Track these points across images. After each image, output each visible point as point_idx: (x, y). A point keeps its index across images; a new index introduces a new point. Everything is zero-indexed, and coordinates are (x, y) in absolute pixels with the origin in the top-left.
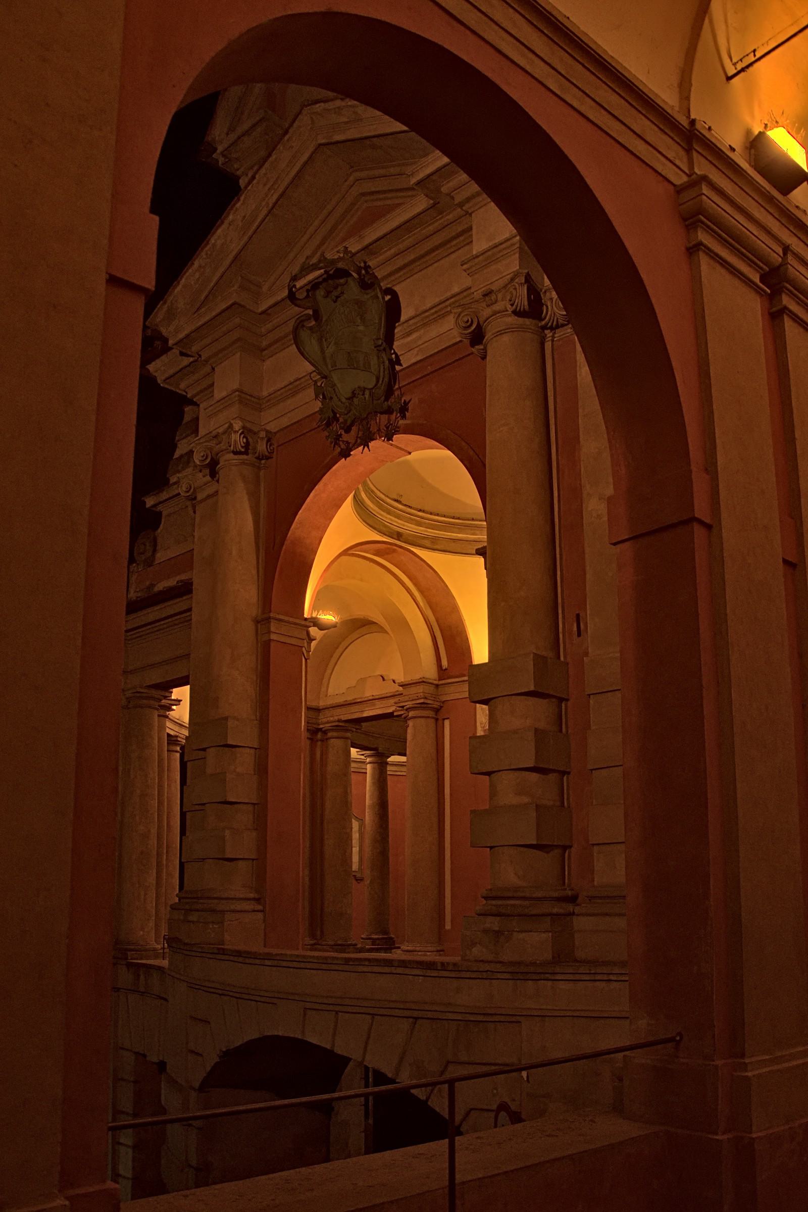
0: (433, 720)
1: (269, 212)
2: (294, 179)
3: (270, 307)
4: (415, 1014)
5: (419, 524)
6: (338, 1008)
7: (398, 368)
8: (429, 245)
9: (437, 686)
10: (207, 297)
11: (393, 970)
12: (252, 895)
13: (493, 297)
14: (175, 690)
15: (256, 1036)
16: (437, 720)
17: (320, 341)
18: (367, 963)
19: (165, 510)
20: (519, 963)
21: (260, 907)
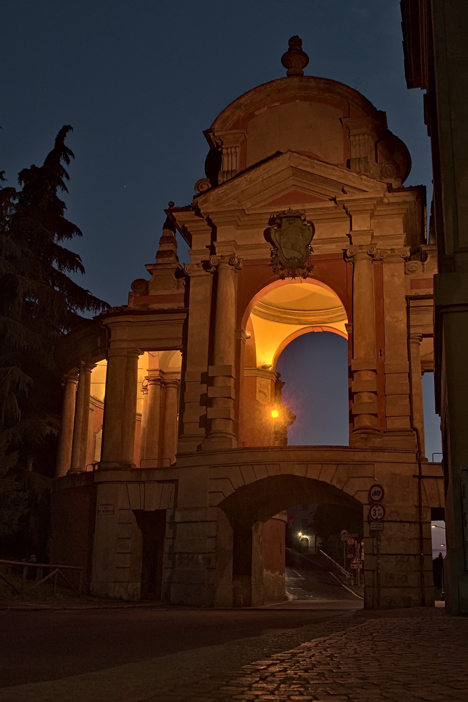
8: (326, 217)
17: (280, 235)
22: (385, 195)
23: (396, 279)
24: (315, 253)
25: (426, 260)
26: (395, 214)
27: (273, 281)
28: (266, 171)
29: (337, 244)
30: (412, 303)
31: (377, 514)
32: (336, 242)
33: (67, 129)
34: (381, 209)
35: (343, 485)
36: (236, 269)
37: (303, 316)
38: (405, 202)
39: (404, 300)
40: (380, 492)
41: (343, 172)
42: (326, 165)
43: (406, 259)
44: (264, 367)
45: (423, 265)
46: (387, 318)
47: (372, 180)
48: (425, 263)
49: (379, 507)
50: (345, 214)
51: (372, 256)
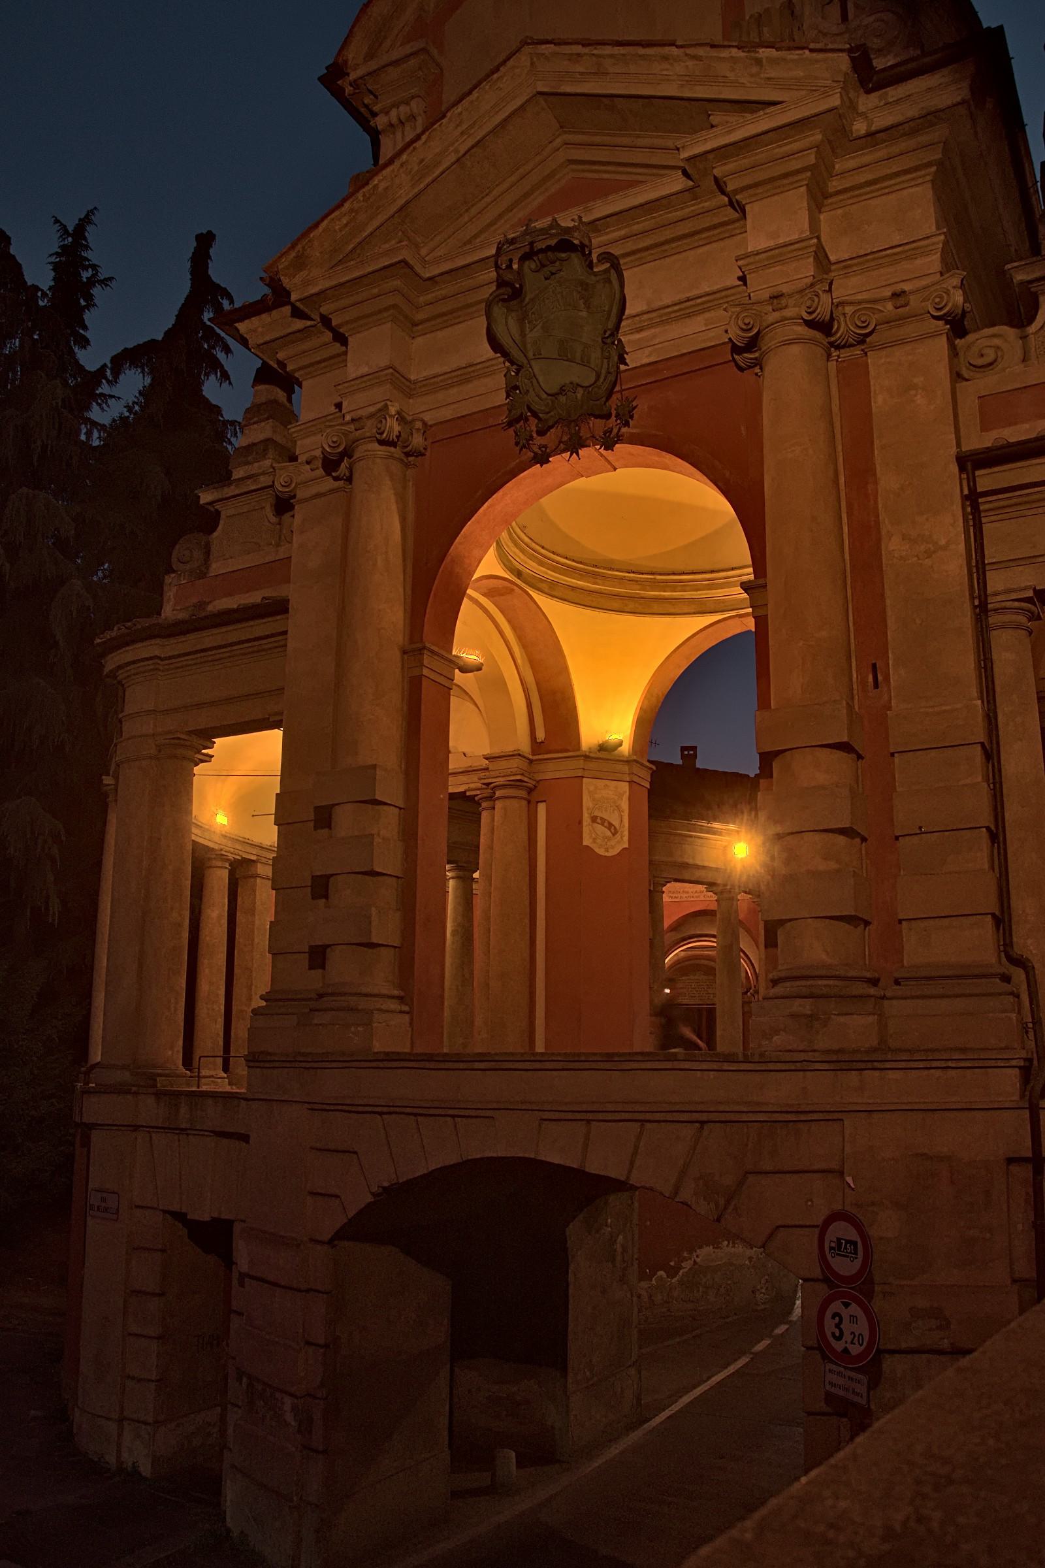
0: (524, 803)
1: (458, 160)
2: (497, 126)
3: (442, 274)
4: (704, 1117)
5: (541, 564)
6: (590, 1116)
7: (622, 367)
8: (668, 234)
9: (531, 761)
10: (354, 248)
11: (676, 1065)
12: (396, 993)
13: (783, 301)
14: (218, 741)
15: (453, 1159)
16: (529, 802)
17: (521, 321)
18: (640, 1058)
19: (226, 511)
20: (840, 1051)
21: (406, 1008)
22: (853, 107)
23: (920, 400)
24: (633, 360)
25: (1031, 320)
26: (897, 174)
27: (513, 474)
28: (464, 126)
29: (707, 315)
30: (986, 479)
31: (847, 1337)
32: (703, 311)
33: (205, 241)
34: (852, 164)
35: (722, 1202)
36: (407, 455)
37: (710, 587)
38: (930, 118)
39: (954, 468)
40: (855, 1244)
41: (695, 57)
42: (641, 51)
43: (957, 326)
44: (606, 750)
45: (1024, 338)
46: (894, 546)
47: (794, 55)
48: (1032, 328)
49: (854, 1309)
50: (730, 210)
51: (824, 327)
